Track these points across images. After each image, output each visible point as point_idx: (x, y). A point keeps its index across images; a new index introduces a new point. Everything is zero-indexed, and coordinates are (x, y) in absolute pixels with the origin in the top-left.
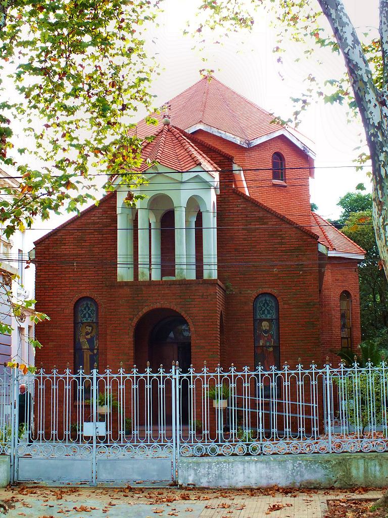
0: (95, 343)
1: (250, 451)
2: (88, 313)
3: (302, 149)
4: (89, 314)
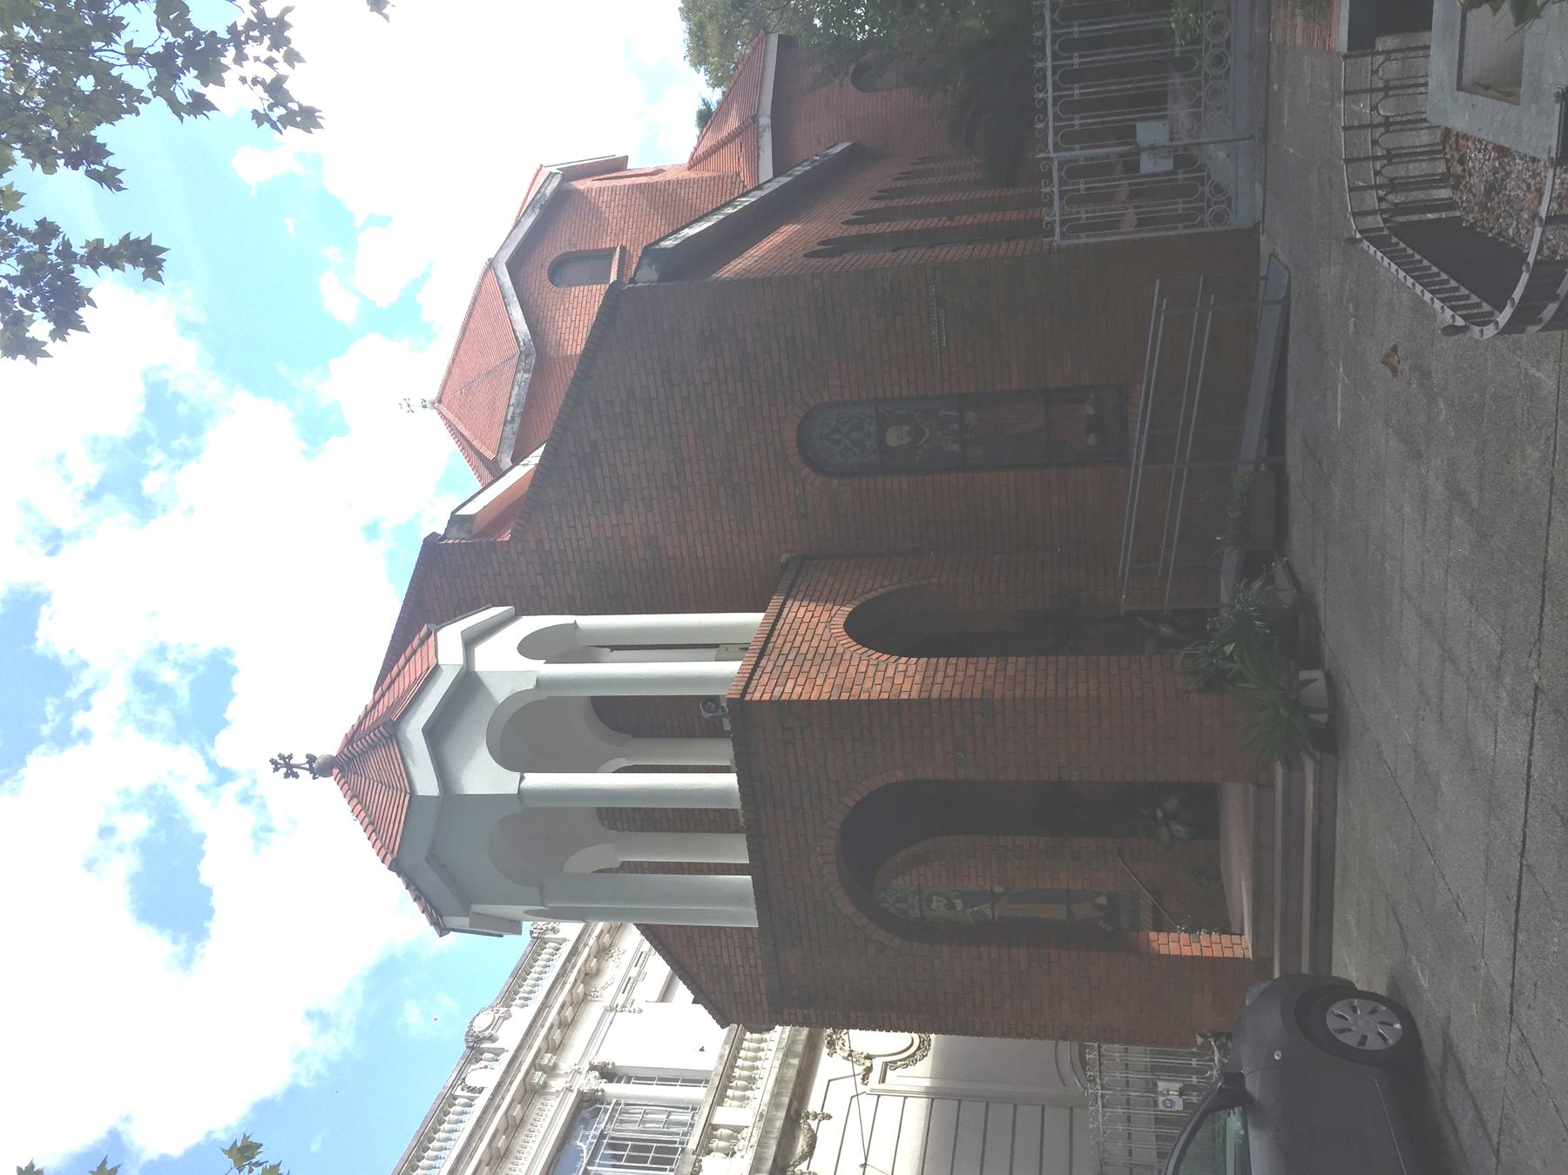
1: (1224, 198)
3: (537, 211)
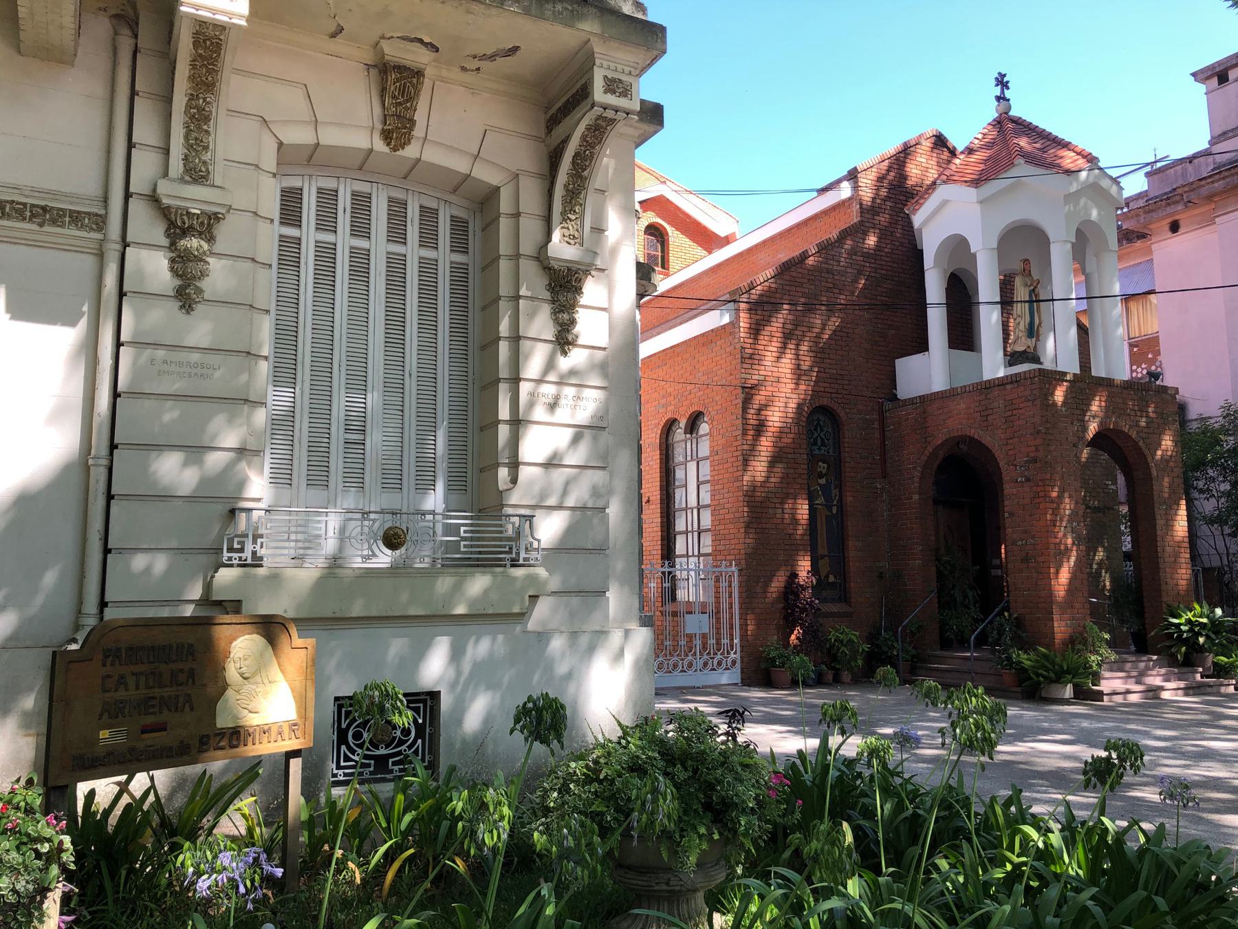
0: (833, 495)
2: (821, 438)
4: (823, 440)
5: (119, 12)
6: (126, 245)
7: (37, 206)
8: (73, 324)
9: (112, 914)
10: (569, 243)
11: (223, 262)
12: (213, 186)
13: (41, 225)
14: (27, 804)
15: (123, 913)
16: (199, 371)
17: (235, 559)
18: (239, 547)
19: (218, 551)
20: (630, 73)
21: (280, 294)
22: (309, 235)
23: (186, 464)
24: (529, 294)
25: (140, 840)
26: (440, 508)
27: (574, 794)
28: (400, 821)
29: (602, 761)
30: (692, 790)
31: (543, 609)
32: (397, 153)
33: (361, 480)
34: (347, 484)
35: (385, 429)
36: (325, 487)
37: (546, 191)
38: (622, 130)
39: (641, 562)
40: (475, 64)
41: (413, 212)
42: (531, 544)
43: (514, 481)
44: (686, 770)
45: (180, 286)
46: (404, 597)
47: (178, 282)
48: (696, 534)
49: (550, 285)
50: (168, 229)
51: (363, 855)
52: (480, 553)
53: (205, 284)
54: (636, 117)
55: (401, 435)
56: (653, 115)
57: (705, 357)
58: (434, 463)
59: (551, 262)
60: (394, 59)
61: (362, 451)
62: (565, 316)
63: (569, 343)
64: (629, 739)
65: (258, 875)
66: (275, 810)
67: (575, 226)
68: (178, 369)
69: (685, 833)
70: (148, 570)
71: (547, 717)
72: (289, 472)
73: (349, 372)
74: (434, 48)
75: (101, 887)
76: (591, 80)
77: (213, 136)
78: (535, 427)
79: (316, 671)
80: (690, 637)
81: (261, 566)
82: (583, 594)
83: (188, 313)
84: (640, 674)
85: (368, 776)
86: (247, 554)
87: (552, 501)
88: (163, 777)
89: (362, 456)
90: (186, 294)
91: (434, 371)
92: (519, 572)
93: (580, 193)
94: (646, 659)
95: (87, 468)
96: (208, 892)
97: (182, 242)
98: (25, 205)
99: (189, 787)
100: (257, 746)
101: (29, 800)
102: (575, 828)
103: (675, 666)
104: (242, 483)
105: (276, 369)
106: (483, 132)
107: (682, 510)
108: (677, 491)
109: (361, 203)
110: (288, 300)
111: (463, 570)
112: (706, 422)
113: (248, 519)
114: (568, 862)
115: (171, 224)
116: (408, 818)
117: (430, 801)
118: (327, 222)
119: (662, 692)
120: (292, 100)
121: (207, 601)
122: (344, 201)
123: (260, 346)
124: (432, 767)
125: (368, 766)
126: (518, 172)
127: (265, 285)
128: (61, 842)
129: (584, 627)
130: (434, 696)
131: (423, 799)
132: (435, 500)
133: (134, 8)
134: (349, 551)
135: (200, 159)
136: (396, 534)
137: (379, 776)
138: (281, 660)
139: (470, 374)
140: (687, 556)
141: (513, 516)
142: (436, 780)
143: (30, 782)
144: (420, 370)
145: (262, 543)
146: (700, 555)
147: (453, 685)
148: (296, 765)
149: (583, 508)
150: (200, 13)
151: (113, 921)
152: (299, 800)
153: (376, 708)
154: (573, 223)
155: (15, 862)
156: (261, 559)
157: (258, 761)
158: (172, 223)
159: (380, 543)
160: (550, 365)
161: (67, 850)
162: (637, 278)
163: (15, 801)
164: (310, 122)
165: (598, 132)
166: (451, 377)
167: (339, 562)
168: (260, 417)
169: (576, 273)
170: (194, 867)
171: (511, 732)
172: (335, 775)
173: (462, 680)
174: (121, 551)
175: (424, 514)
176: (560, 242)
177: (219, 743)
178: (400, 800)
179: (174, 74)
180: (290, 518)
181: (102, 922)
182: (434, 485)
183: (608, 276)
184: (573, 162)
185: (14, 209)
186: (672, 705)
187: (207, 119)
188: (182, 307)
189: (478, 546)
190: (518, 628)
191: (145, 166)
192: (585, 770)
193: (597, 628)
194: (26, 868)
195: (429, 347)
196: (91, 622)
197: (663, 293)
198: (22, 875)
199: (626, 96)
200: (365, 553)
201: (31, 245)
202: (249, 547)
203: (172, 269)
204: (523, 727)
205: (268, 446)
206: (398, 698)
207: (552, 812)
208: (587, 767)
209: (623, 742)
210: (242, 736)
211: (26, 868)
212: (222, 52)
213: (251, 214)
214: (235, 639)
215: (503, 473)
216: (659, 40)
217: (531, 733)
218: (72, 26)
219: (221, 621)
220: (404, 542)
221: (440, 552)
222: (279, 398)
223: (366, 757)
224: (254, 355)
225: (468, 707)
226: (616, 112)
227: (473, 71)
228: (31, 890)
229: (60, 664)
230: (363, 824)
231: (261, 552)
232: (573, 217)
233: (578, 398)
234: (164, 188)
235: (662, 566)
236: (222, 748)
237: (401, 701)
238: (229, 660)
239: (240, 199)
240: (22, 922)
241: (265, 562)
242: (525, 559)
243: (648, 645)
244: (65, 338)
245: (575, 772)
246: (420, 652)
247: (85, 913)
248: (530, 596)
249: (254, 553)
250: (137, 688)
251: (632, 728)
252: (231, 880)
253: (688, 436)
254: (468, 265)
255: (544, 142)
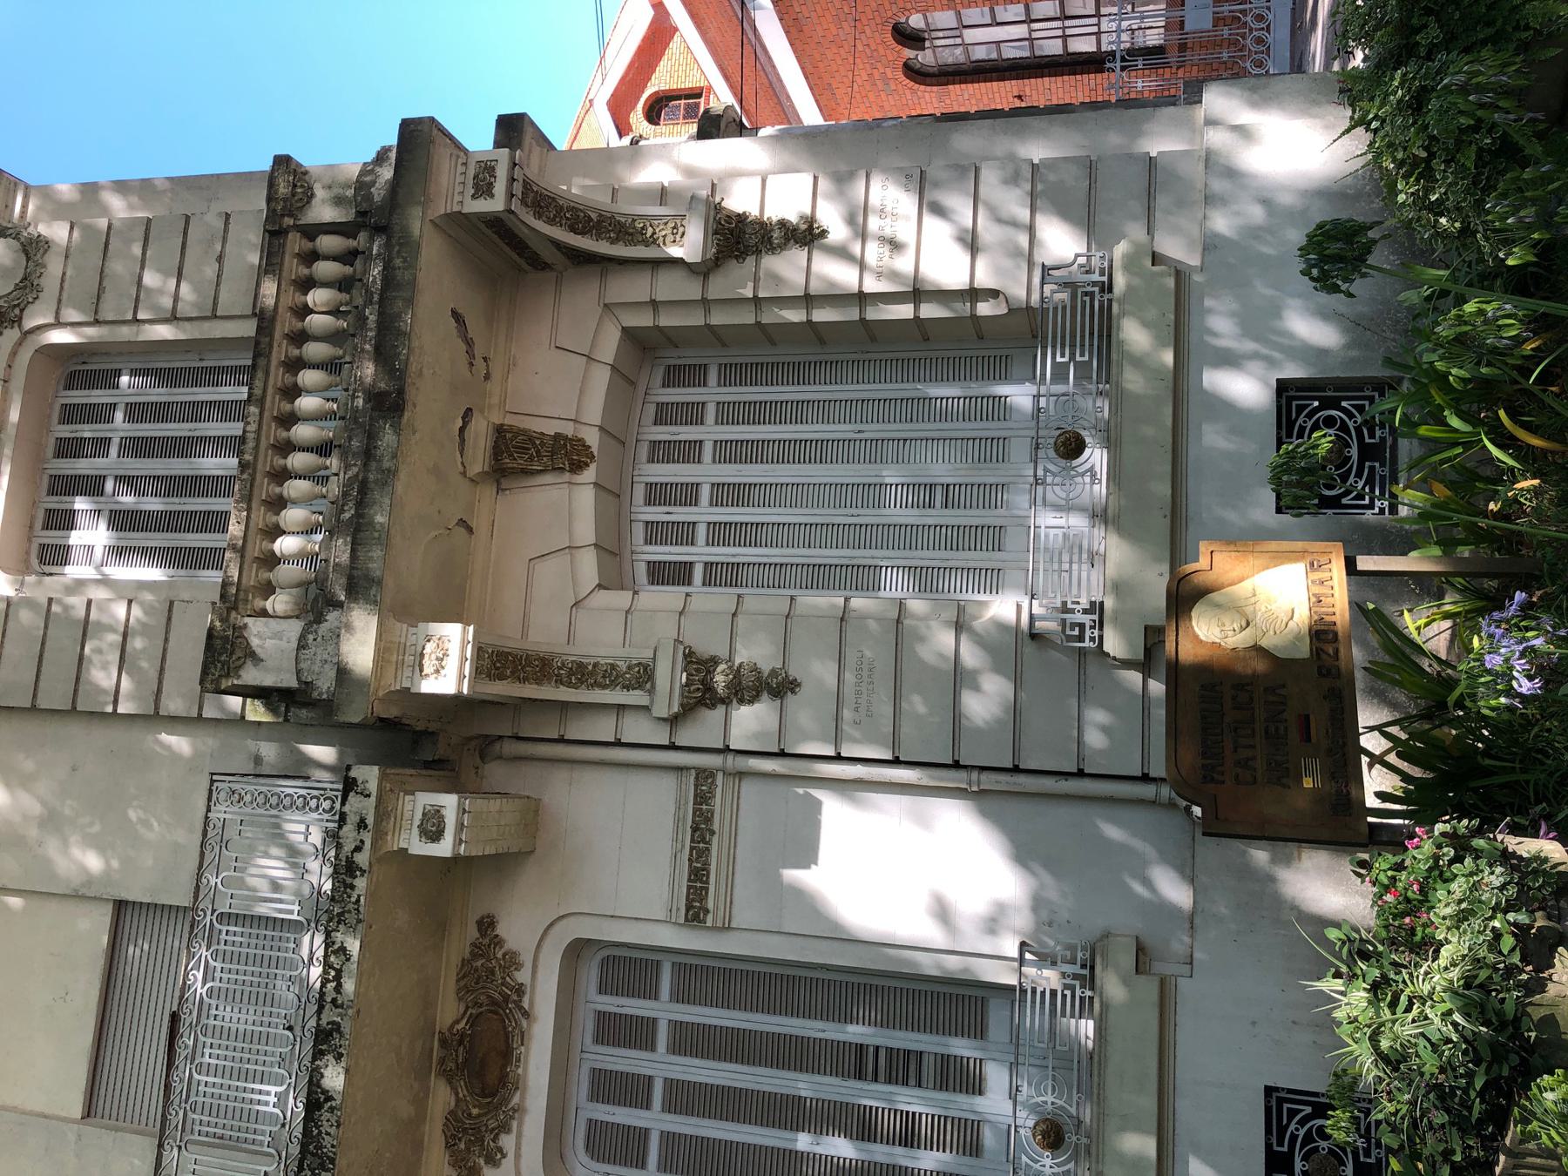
5: (477, 752)
6: (727, 750)
7: (692, 836)
8: (819, 803)
9: (1542, 776)
10: (683, 234)
11: (739, 646)
12: (654, 659)
13: (713, 833)
14: (1389, 869)
15: (1543, 764)
16: (865, 673)
17: (1092, 633)
18: (1077, 629)
19: (1082, 652)
20: (465, 164)
21: (771, 584)
22: (700, 553)
23: (976, 688)
24: (751, 285)
25: (1447, 743)
26: (1029, 388)
27: (1445, 193)
28: (1456, 431)
29: (1400, 155)
30: (1457, 15)
31: (1174, 247)
32: (596, 454)
33: (994, 487)
34: (999, 503)
35: (929, 460)
36: (1003, 530)
37: (622, 267)
38: (536, 171)
39: (1105, 105)
40: (479, 362)
41: (663, 433)
42: (1081, 266)
43: (994, 294)
44: (1425, 26)
45: (769, 693)
46: (1148, 431)
47: (765, 696)
48: (1068, 23)
49: (737, 257)
50: (706, 706)
51: (1503, 476)
52: (1091, 334)
53: (766, 668)
54: (517, 153)
55: (936, 441)
56: (512, 128)
57: (819, 29)
58: (971, 398)
59: (708, 257)
60: (487, 460)
61: (957, 487)
62: (775, 236)
63: (811, 228)
64: (1371, 116)
65: (1521, 621)
66: (1424, 587)
67: (661, 227)
68: (864, 696)
69: (1522, 23)
70: (1105, 729)
71: (1334, 248)
72: (983, 572)
73: (860, 505)
74: (467, 415)
75: (1502, 786)
76: (480, 216)
77: (599, 659)
78: (922, 269)
79: (1245, 539)
80: (1218, 21)
81: (1102, 604)
82: (1152, 191)
83: (799, 685)
84: (1270, 98)
85: (1387, 469)
86: (1086, 619)
87: (1023, 240)
88: (1368, 715)
89: (963, 487)
90: (778, 687)
91: (854, 403)
92: (1120, 281)
93: (619, 222)
94: (1249, 89)
95: (982, 793)
96: (1537, 681)
97: (720, 691)
98: (692, 849)
99: (1381, 685)
100: (1337, 610)
101: (1385, 866)
102: (1508, 206)
103: (1259, 41)
104: (1001, 626)
105: (860, 587)
106: (557, 350)
107: (1032, 47)
108: (1005, 56)
109: (658, 494)
110: (778, 574)
111: (1114, 356)
112: (908, 18)
113: (1043, 618)
114: (1557, 214)
115: (701, 703)
116: (1455, 422)
117: (1433, 392)
118: (683, 533)
119: (1297, 59)
120: (549, 573)
121: (1146, 664)
122: (657, 514)
123: (834, 606)
124: (1382, 387)
125: (1372, 469)
126: (602, 305)
127: (761, 602)
128: (1443, 834)
129: (1200, 186)
130: (1283, 387)
131: (1428, 400)
132: (1020, 395)
133: (470, 739)
134: (1085, 499)
135: (626, 673)
136: (1064, 444)
137: (1388, 455)
138: (1226, 583)
139: (854, 356)
140: (1098, 34)
141: (1042, 292)
142: (1400, 380)
143: (1362, 864)
144: (853, 420)
145: (1073, 603)
146: (1098, 15)
147: (1271, 362)
148: (1365, 563)
149: (1033, 196)
150: (467, 673)
151: (1551, 774)
152: (1414, 558)
153: (1306, 479)
154: (657, 231)
155: (1465, 886)
156: (1092, 604)
157: (1357, 606)
158: (700, 701)
159: (1075, 462)
160: (841, 253)
161: (1455, 828)
162: (718, 136)
163: (1386, 881)
164: (571, 554)
165: (542, 202)
166: (861, 381)
167: (1099, 510)
168: (917, 606)
169: (720, 224)
170: (1500, 696)
171: (1351, 295)
172: (1382, 511)
173: (1265, 351)
174: (1080, 758)
175: (1039, 410)
176: (682, 246)
177: (1329, 655)
178: (1427, 430)
179: (536, 700)
180: (1041, 570)
181: (1551, 786)
182: (1000, 397)
183: (720, 179)
184: (582, 233)
185: (697, 859)
186: (1317, 43)
187: (581, 665)
188: (793, 692)
189: (1083, 337)
190: (1197, 278)
191: (638, 729)
192: (1412, 180)
193: (1201, 166)
194: (1471, 874)
195: (824, 411)
196: (1166, 791)
197: (735, 94)
198: (1483, 878)
199: (493, 169)
200: (1087, 479)
201: (735, 843)
202: (1079, 618)
203: (751, 702)
204: (1345, 280)
205: (952, 596)
206: (1293, 450)
207: (1469, 223)
208: (1406, 177)
209: (1374, 125)
210: (1323, 627)
211: (1471, 874)
212: (506, 650)
213: (682, 617)
214: (1196, 637)
215: (984, 309)
216: (419, 128)
217: (1356, 269)
218: (498, 801)
219: (1174, 653)
220: (1075, 432)
221: (1090, 386)
222: (895, 585)
223: (1359, 475)
224: (844, 612)
225: (1302, 341)
226: (514, 180)
227: (488, 366)
228: (1503, 870)
229: (1217, 827)
230: (1454, 476)
231: (1084, 603)
232: (650, 230)
233: (882, 212)
234: (661, 710)
235: (1113, 71)
236: (1337, 651)
237: (1298, 446)
238: (1223, 644)
239: (666, 630)
240: (1544, 881)
241: (1097, 598)
242: (1102, 274)
243: (1228, 89)
244: (834, 811)
245: (1412, 194)
246: (1223, 408)
247: (1538, 809)
248: (1153, 265)
249: (1085, 612)
250: (1253, 747)
251: (1354, 112)
252: (1522, 655)
253: (927, 44)
254: (720, 365)
255: (561, 273)
